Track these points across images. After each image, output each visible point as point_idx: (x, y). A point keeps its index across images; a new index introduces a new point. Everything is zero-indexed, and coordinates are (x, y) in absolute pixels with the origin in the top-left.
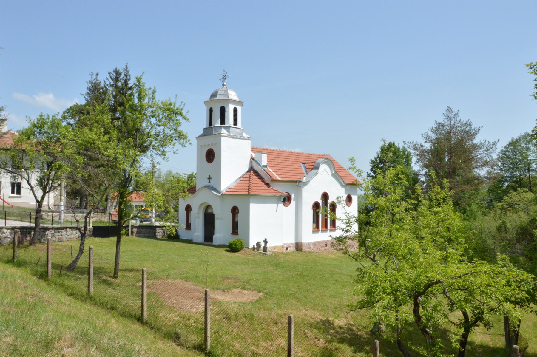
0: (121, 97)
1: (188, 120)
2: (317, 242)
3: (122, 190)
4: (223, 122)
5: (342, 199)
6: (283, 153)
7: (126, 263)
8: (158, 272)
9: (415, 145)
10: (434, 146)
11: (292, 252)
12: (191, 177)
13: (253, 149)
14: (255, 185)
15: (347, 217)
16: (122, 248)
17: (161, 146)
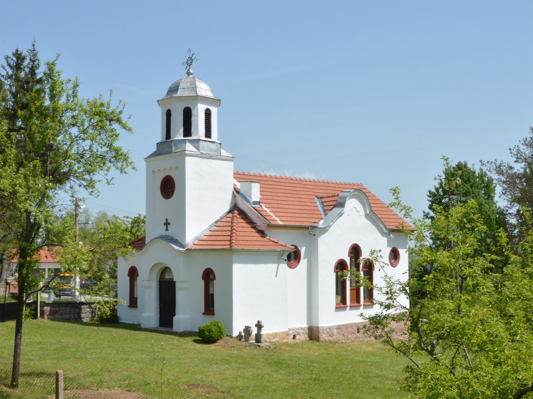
0: (24, 95)
1: (130, 129)
2: (344, 325)
3: (24, 244)
4: (188, 132)
5: (379, 254)
6: (287, 181)
7: (32, 363)
8: (84, 376)
9: (500, 166)
10: (530, 168)
11: (303, 342)
12: (137, 222)
13: (237, 176)
14: (241, 234)
15: (388, 283)
16: (25, 339)
17: (88, 172)
